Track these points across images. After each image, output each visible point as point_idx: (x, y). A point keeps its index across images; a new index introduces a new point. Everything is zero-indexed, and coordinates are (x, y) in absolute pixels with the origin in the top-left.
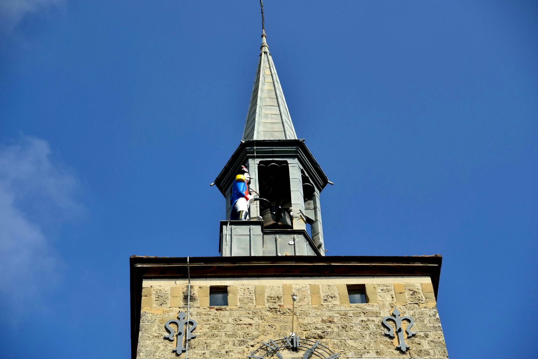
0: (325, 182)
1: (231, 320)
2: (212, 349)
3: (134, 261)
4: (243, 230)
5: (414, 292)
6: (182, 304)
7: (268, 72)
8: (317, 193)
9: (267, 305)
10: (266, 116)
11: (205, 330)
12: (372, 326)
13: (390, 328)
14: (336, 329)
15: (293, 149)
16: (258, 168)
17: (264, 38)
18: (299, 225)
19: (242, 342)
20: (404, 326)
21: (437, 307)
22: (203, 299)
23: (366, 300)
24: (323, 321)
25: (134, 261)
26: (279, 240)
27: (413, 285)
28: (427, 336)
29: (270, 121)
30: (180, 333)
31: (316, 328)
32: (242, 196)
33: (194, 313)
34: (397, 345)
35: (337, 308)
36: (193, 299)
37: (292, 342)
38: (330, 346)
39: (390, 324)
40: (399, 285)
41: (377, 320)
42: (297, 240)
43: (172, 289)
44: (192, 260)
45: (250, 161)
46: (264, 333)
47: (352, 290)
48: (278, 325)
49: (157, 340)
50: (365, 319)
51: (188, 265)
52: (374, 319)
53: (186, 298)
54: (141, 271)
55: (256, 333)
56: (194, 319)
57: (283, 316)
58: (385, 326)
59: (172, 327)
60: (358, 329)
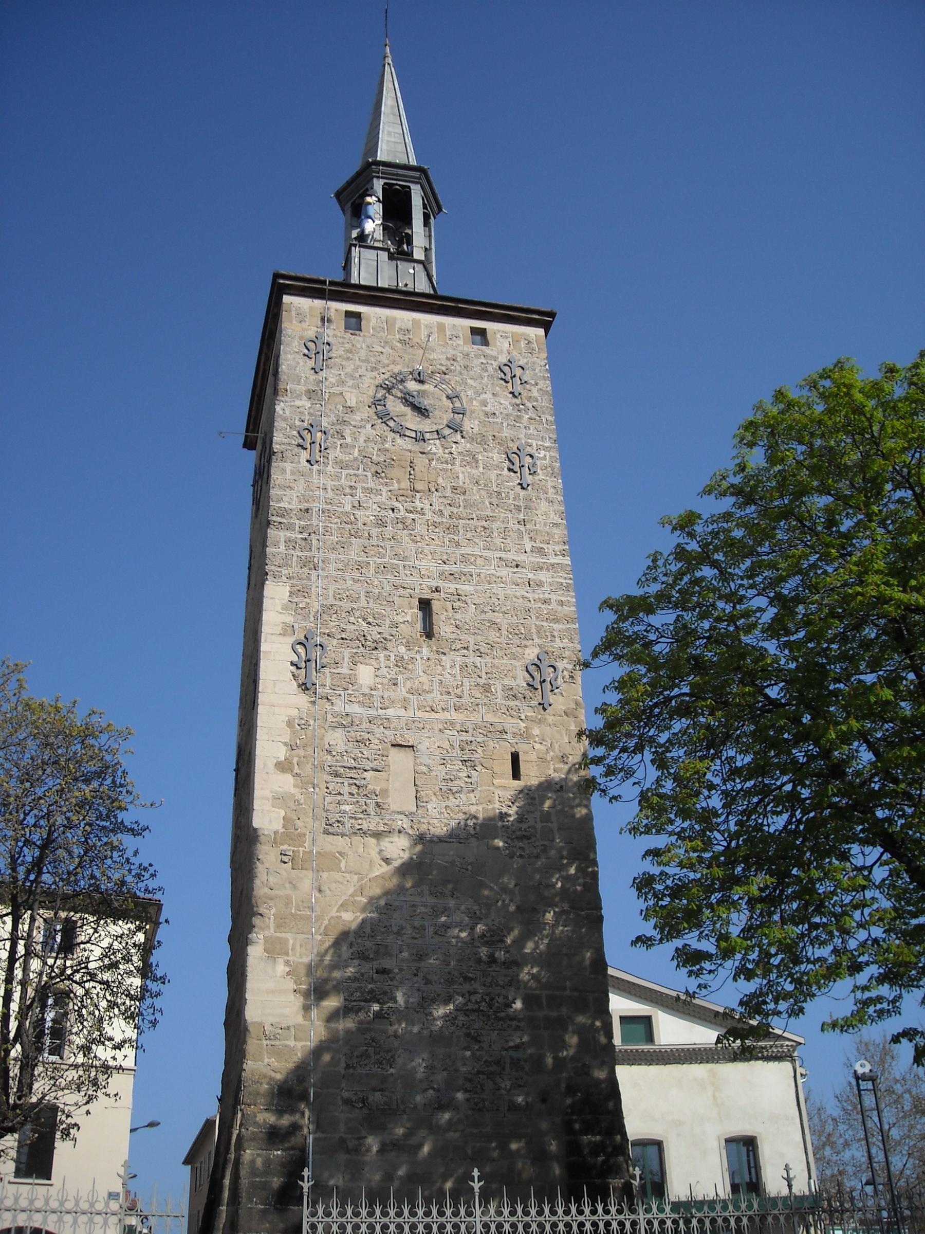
0: (440, 210)
1: (364, 346)
2: (347, 371)
3: (277, 276)
4: (369, 254)
5: (529, 342)
6: (319, 323)
7: (391, 86)
8: (432, 220)
9: (397, 336)
10: (389, 134)
11: (341, 352)
12: (490, 369)
13: (507, 373)
14: (458, 368)
15: (417, 174)
16: (383, 189)
17: (388, 48)
18: (418, 255)
19: (374, 369)
20: (518, 372)
21: (548, 358)
22: (339, 323)
23: (486, 343)
24: (447, 359)
25: (277, 276)
26: (400, 267)
27: (528, 335)
28: (537, 384)
29: (393, 140)
30: (317, 351)
31: (441, 365)
32: (370, 217)
33: (331, 334)
34: (511, 390)
35: (460, 348)
36: (329, 321)
37: (419, 374)
38: (452, 383)
39: (506, 369)
40: (517, 333)
41: (495, 364)
42: (416, 269)
43: (311, 308)
44: (331, 283)
45: (375, 180)
46: (394, 362)
47: (474, 331)
48: (406, 357)
49: (298, 356)
50: (484, 362)
51: (327, 287)
52: (493, 362)
53: (323, 319)
54: (280, 287)
55: (387, 362)
56: (330, 340)
57: (411, 350)
58: (502, 371)
59: (311, 345)
60: (478, 370)
